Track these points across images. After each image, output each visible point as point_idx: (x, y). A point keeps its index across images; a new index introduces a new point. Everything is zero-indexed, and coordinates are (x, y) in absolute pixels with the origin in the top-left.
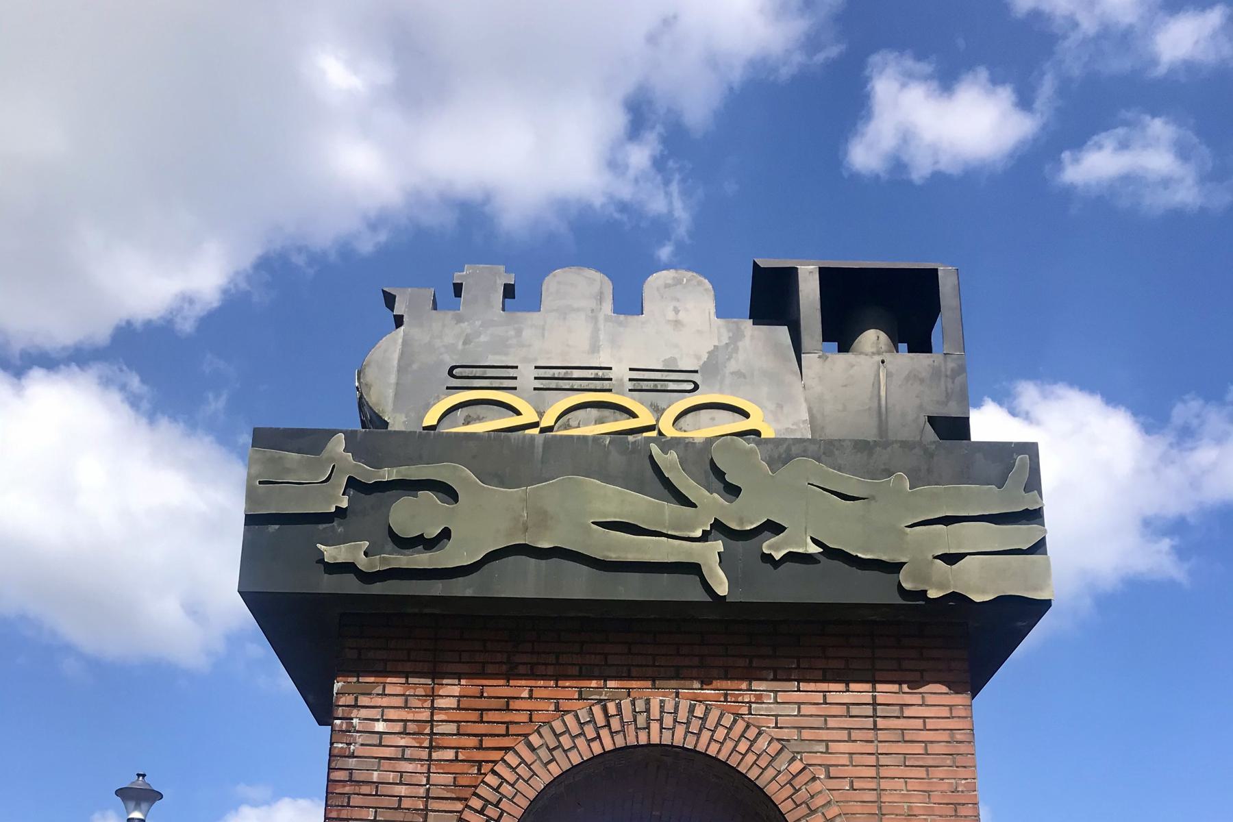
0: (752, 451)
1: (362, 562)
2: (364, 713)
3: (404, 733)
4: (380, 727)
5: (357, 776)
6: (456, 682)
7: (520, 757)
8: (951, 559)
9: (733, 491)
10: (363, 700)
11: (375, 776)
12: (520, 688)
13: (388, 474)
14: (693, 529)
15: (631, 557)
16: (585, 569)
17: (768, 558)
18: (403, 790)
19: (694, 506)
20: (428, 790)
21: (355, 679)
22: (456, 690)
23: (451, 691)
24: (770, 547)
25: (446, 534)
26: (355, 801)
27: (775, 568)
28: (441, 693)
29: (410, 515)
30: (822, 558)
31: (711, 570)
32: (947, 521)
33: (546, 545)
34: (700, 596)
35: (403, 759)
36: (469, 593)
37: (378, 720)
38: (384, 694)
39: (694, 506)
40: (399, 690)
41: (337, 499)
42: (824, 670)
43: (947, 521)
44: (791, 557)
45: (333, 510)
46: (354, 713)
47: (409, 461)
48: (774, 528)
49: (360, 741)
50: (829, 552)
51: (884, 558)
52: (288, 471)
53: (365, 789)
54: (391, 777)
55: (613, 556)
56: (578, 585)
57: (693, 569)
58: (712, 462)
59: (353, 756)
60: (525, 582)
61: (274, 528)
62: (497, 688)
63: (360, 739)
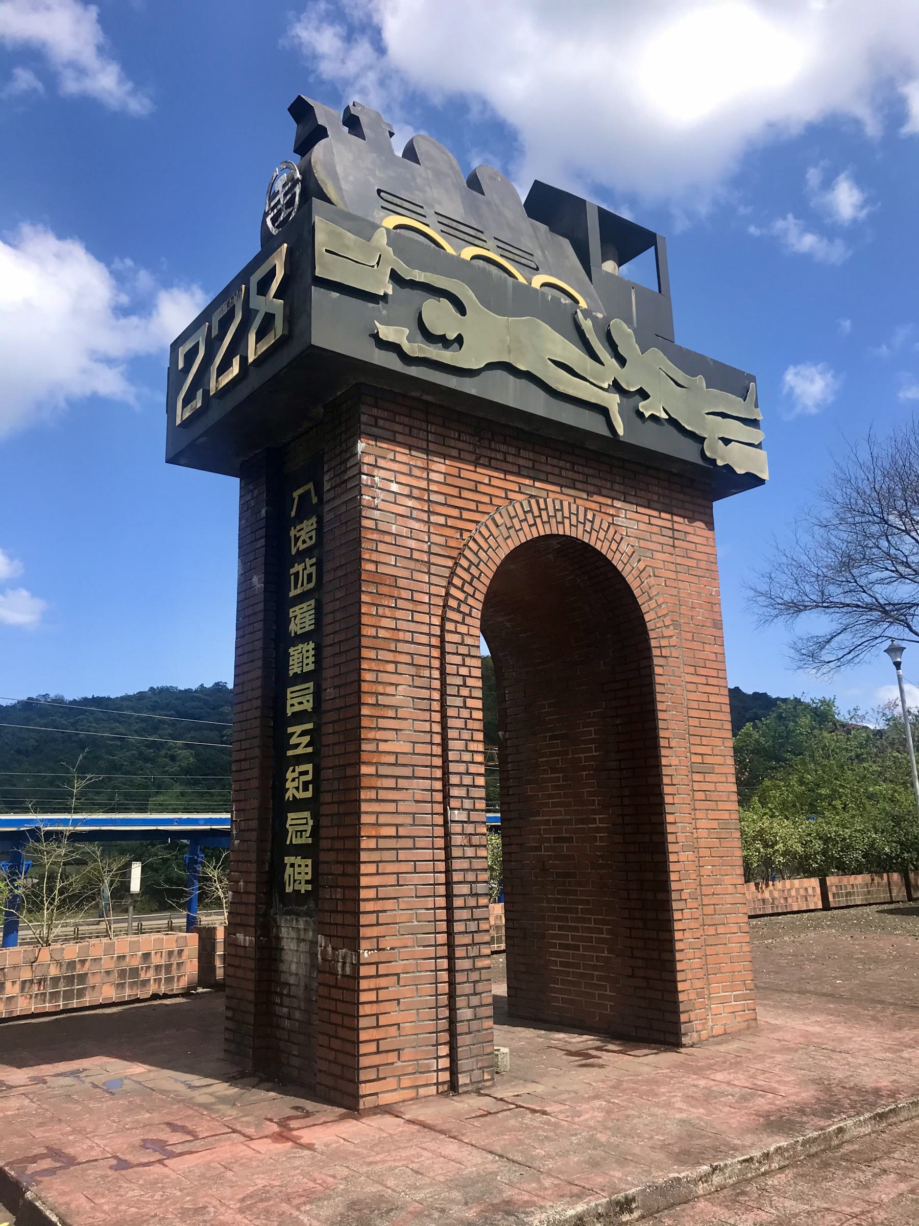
0: (629, 335)
1: (406, 347)
2: (383, 473)
3: (409, 496)
4: (394, 487)
5: (382, 526)
6: (442, 461)
7: (490, 531)
8: (727, 441)
9: (622, 361)
10: (381, 462)
11: (394, 529)
12: (482, 475)
13: (419, 276)
14: (604, 382)
15: (571, 392)
16: (541, 394)
17: (640, 415)
18: (413, 544)
19: (602, 364)
20: (430, 546)
21: (373, 443)
22: (442, 468)
23: (440, 466)
24: (642, 407)
25: (459, 340)
26: (381, 547)
27: (643, 423)
28: (433, 468)
29: (440, 317)
30: (665, 423)
31: (615, 416)
32: (724, 415)
33: (689, 428)
34: (604, 431)
35: (411, 518)
36: (473, 392)
37: (392, 481)
38: (394, 460)
39: (602, 364)
40: (404, 459)
41: (385, 286)
42: (649, 501)
43: (724, 415)
44: (653, 417)
45: (382, 294)
46: (375, 472)
47: (434, 271)
48: (643, 394)
49: (381, 497)
50: (672, 421)
51: (697, 432)
52: (347, 247)
53: (388, 538)
54: (405, 532)
55: (561, 388)
56: (537, 404)
57: (604, 411)
58: (609, 331)
59: (376, 508)
60: (508, 393)
61: (335, 295)
62: (470, 473)
63: (382, 495)
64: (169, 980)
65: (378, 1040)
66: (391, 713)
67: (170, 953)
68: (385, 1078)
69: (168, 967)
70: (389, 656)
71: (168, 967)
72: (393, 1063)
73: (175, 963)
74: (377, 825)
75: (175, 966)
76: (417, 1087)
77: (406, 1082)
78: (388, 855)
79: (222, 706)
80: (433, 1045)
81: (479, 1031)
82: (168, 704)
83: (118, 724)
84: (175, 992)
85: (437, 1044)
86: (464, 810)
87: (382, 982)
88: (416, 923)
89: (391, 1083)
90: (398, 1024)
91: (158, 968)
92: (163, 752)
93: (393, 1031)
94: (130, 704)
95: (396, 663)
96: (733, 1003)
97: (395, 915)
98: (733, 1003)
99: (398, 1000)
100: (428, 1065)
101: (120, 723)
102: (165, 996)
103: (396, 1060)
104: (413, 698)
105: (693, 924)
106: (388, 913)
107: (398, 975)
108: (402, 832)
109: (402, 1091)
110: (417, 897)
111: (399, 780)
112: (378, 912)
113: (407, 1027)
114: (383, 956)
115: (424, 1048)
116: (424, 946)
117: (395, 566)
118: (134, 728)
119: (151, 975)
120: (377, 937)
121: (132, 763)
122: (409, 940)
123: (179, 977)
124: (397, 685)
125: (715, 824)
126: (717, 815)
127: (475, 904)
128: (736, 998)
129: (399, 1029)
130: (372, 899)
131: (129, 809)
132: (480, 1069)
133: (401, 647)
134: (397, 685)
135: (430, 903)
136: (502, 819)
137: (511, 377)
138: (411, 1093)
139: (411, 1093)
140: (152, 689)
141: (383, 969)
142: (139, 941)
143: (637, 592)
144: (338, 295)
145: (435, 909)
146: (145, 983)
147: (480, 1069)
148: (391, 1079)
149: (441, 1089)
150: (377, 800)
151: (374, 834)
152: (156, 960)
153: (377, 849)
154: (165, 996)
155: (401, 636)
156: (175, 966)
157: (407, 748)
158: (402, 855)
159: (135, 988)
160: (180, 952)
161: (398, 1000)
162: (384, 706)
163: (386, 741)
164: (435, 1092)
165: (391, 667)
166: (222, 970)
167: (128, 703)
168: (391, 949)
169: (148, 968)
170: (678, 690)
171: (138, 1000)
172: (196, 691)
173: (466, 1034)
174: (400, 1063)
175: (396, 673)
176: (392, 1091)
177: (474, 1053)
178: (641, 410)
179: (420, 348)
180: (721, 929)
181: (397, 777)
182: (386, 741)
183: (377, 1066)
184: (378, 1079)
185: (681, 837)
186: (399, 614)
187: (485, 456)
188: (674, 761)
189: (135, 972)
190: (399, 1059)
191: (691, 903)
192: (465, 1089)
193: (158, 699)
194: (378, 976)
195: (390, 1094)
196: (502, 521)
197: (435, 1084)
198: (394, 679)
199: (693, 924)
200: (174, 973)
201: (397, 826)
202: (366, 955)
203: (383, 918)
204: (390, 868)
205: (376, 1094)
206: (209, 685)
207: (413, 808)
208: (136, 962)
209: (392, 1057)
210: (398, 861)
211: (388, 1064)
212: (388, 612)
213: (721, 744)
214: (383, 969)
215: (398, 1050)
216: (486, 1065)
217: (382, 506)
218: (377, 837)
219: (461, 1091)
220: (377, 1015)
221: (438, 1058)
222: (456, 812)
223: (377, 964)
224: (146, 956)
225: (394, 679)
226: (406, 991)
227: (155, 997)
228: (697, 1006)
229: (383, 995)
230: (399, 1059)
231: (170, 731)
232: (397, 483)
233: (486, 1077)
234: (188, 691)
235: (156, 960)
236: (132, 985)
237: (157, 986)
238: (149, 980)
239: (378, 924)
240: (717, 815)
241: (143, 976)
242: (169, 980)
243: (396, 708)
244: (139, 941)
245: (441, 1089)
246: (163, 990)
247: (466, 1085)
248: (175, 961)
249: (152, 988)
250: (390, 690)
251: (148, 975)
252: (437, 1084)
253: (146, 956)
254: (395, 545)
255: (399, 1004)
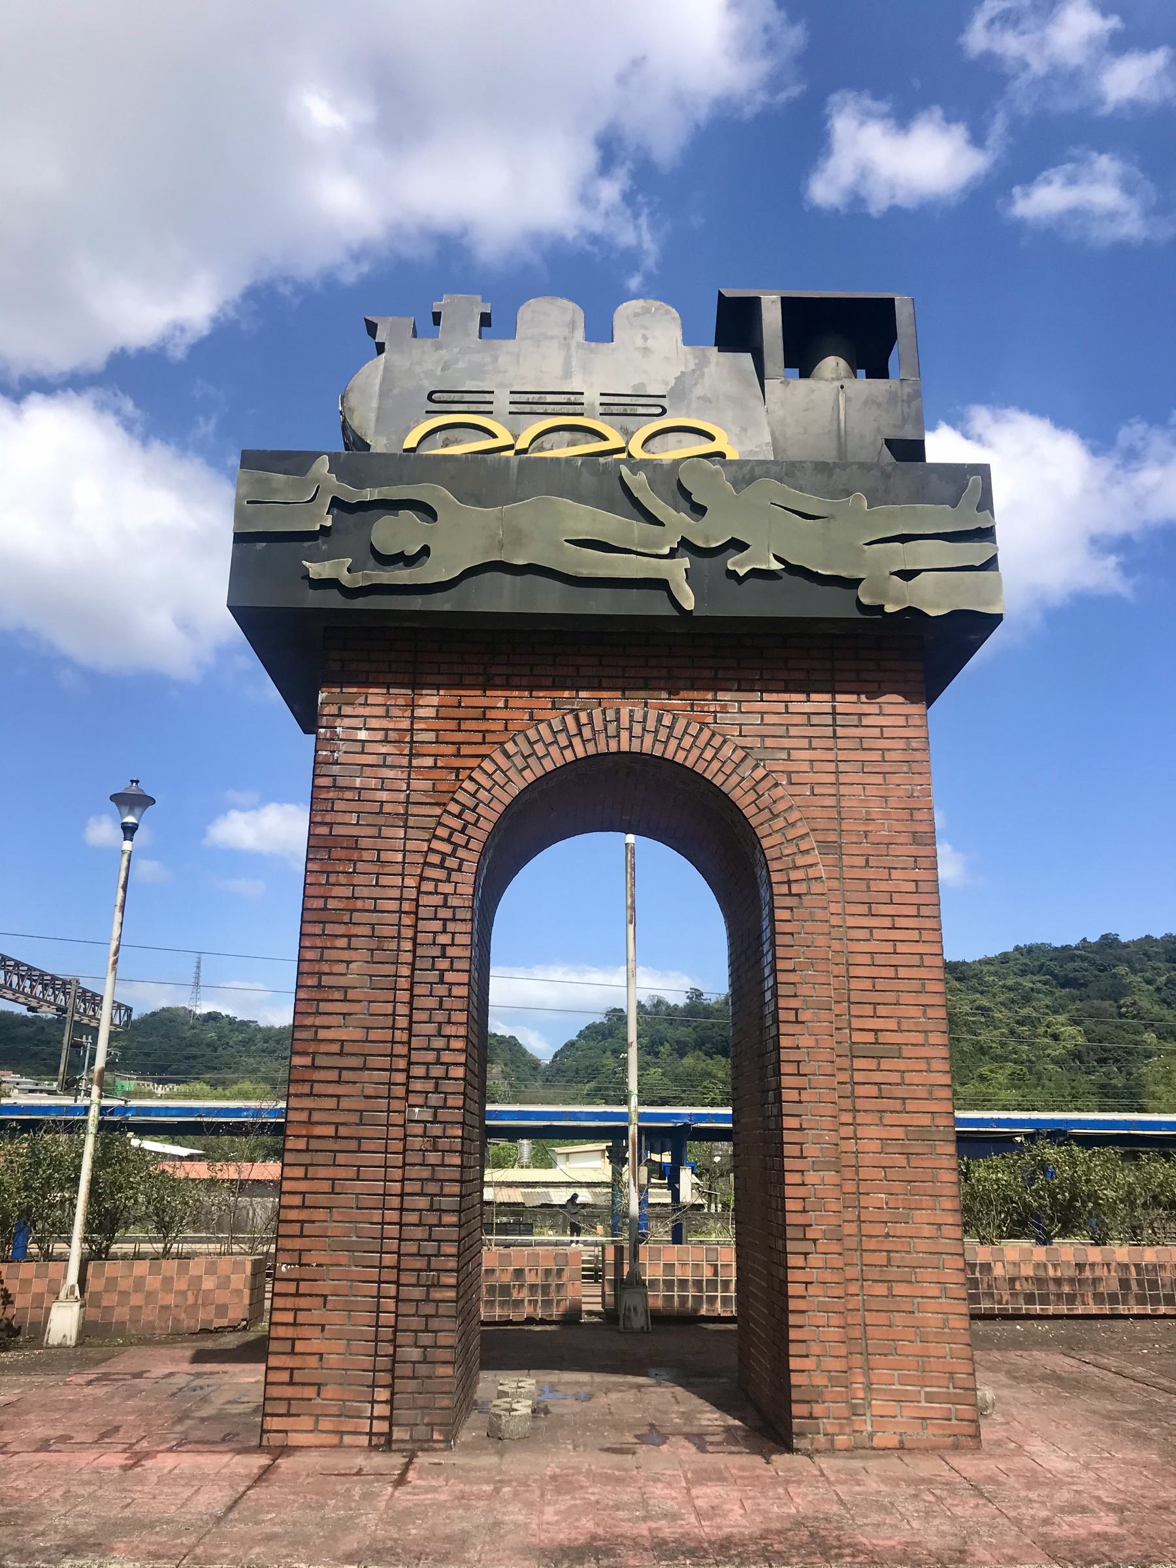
0: (717, 472)
1: (346, 578)
2: (347, 722)
3: (385, 741)
4: (362, 735)
5: (341, 782)
6: (435, 692)
8: (907, 575)
9: (699, 510)
13: (370, 494)
14: (661, 547)
15: (602, 573)
16: (558, 585)
17: (732, 574)
18: (384, 796)
19: (662, 524)
21: (338, 690)
22: (435, 701)
23: (430, 701)
24: (734, 564)
25: (425, 551)
26: (339, 806)
28: (420, 703)
29: (391, 533)
30: (784, 575)
32: (903, 539)
34: (667, 610)
35: (384, 766)
36: (447, 607)
37: (360, 729)
38: (366, 704)
39: (662, 524)
41: (321, 518)
43: (903, 539)
46: (338, 722)
48: (738, 546)
49: (343, 748)
50: (791, 569)
51: (844, 574)
52: (275, 491)
53: (348, 795)
54: (373, 783)
55: (585, 572)
56: (551, 600)
57: (661, 584)
60: (501, 597)
62: (474, 698)
63: (343, 746)
64: (547, 1304)
65: (292, 1369)
66: (338, 995)
67: (548, 1272)
68: (299, 1415)
69: (546, 1289)
70: (340, 929)
71: (546, 1289)
72: (310, 1399)
73: (554, 1284)
74: (310, 1123)
75: (553, 1288)
76: (342, 1433)
77: (325, 1424)
78: (320, 1158)
79: (1114, 967)
80: (368, 1386)
81: (430, 1378)
82: (1041, 967)
83: (978, 995)
84: (554, 1318)
85: (373, 1386)
86: (428, 1107)
87: (303, 1302)
88: (354, 1239)
89: (306, 1422)
90: (321, 1354)
91: (533, 1288)
92: (1041, 1030)
93: (313, 1361)
94: (992, 969)
95: (349, 937)
96: (923, 1404)
97: (326, 1228)
98: (923, 1404)
99: (323, 1326)
100: (358, 1409)
101: (982, 993)
102: (542, 1322)
103: (314, 1396)
104: (371, 976)
105: (828, 1276)
106: (317, 1224)
107: (325, 1296)
108: (343, 1131)
109: (320, 1435)
110: (358, 1208)
111: (344, 1073)
112: (302, 1222)
113: (332, 1360)
114: (306, 1273)
115: (354, 1388)
116: (364, 1267)
117: (358, 824)
118: (999, 1000)
119: (524, 1294)
120: (300, 1251)
121: (1003, 1045)
122: (343, 1257)
123: (559, 1302)
124: (348, 963)
125: (899, 1133)
126: (905, 1119)
127: (436, 1222)
128: (930, 1398)
129: (321, 1359)
130: (297, 1207)
131: (976, 1105)
132: (427, 1425)
133: (357, 917)
134: (348, 963)
135: (377, 1216)
136: (734, 1118)
137: (508, 577)
138: (334, 1439)
139: (334, 1439)
140: (1017, 948)
141: (304, 1287)
142: (509, 1255)
143: (749, 812)
144: (264, 544)
145: (383, 1223)
146: (518, 1303)
147: (427, 1425)
148: (306, 1418)
149: (375, 1441)
150: (311, 1095)
151: (304, 1132)
152: (530, 1279)
153: (307, 1150)
154: (542, 1322)
155: (359, 904)
156: (553, 1288)
157: (358, 1034)
158: (341, 1158)
159: (506, 1309)
160: (560, 1272)
161: (323, 1326)
162: (330, 987)
163: (329, 1027)
164: (366, 1443)
165: (342, 942)
166: (612, 1298)
167: (988, 967)
168: (317, 1265)
169: (521, 1286)
170: (821, 941)
171: (510, 1322)
172: (1077, 948)
173: (408, 1378)
174: (319, 1401)
175: (349, 948)
176: (306, 1431)
177: (421, 1403)
178: (731, 568)
179: (366, 577)
180: (899, 1289)
181: (341, 1069)
182: (329, 1027)
183: (289, 1400)
184: (288, 1415)
185: (811, 1150)
186: (358, 879)
187: (500, 675)
188: (806, 1041)
189: (505, 1289)
190: (318, 1395)
191: (822, 1245)
192: (402, 1446)
193: (1027, 961)
194: (297, 1295)
195: (305, 1435)
196: (516, 750)
197: (367, 1434)
198: (346, 955)
199: (828, 1276)
200: (553, 1295)
201: (337, 1125)
202: (283, 1268)
203: (309, 1229)
204: (322, 1172)
205: (286, 1432)
206: (1093, 938)
207: (361, 1104)
208: (506, 1278)
209: (310, 1392)
210: (335, 1165)
211: (303, 1399)
212: (342, 879)
213: (920, 1014)
214: (304, 1287)
215: (319, 1385)
216: (438, 1421)
217: (344, 758)
218: (309, 1137)
219: (394, 1446)
220: (293, 1340)
221: (373, 1402)
222: (417, 1110)
223: (298, 1281)
224: (519, 1273)
225: (346, 955)
226: (336, 1317)
227: (530, 1321)
228: (828, 1397)
229: (302, 1317)
230: (318, 1395)
231: (1047, 1002)
232: (367, 729)
233: (436, 1436)
234: (1066, 948)
235: (530, 1279)
236: (503, 1304)
237: (532, 1309)
238: (522, 1301)
239: (302, 1236)
240: (905, 1119)
241: (515, 1295)
242: (547, 1304)
243: (346, 989)
244: (509, 1255)
245: (375, 1441)
246: (540, 1313)
247: (403, 1441)
248: (553, 1281)
249: (527, 1311)
250: (341, 968)
251: (522, 1295)
252: (370, 1434)
253: (519, 1273)
254: (359, 800)
255: (323, 1330)
